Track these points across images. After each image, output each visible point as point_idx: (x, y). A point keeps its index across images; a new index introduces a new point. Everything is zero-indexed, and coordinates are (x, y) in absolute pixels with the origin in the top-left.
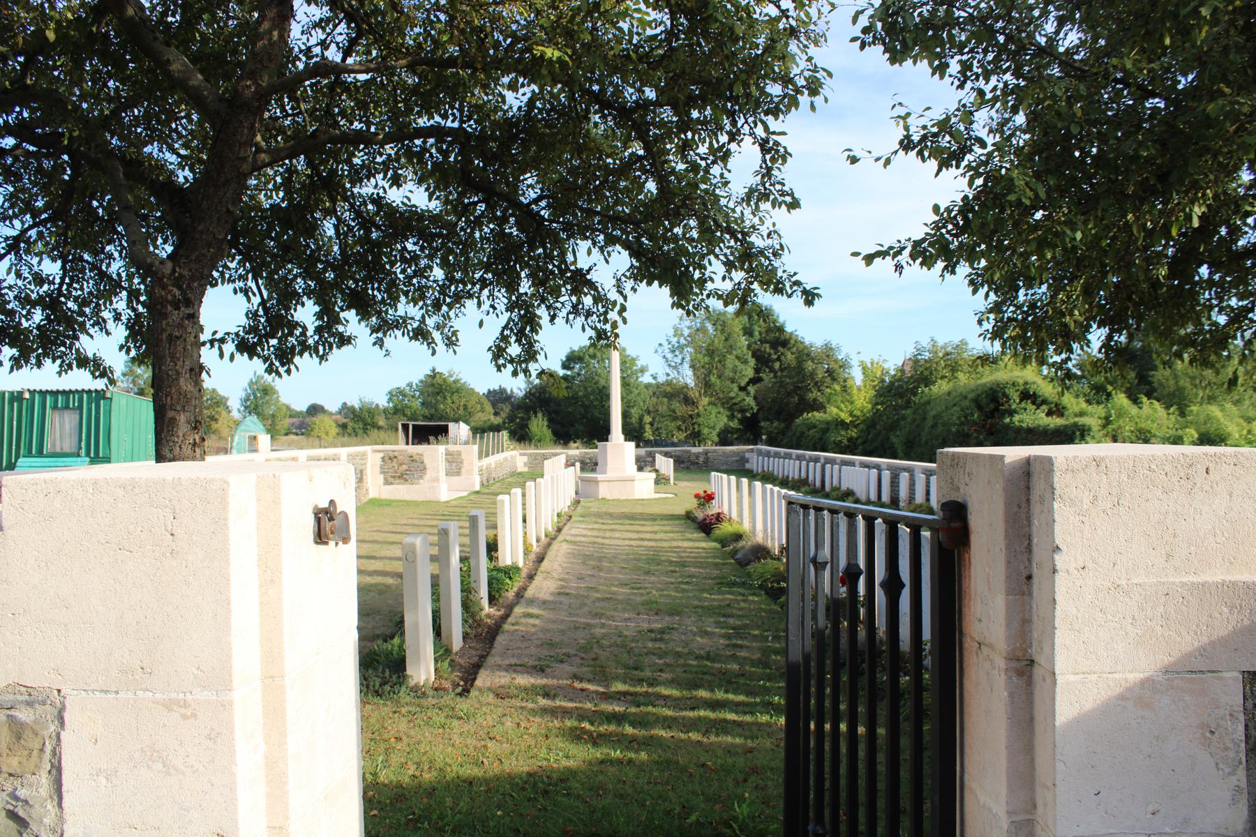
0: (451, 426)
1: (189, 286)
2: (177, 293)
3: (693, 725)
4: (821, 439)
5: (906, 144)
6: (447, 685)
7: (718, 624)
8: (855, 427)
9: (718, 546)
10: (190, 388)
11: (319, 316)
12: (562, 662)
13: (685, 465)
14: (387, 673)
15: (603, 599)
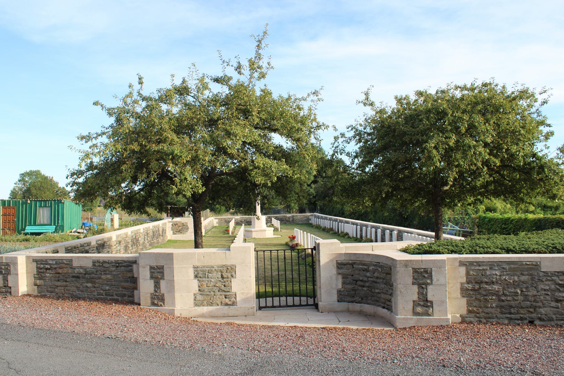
4: (342, 209)
13: (284, 221)
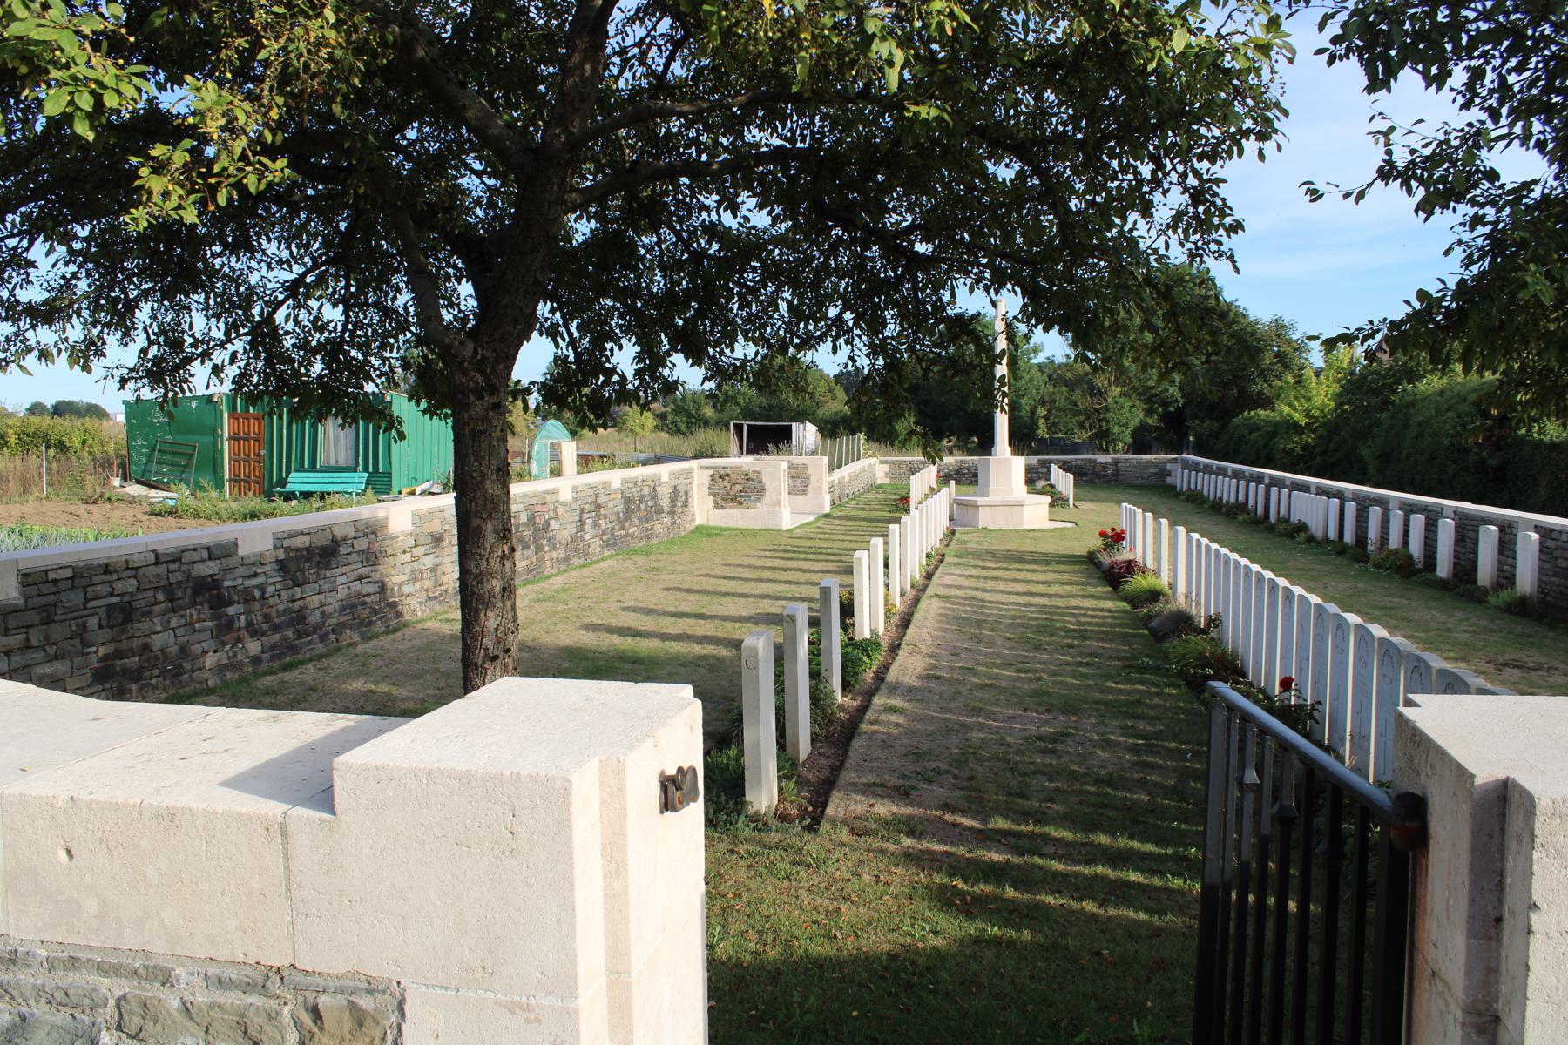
0: (795, 426)
1: (493, 370)
2: (479, 378)
3: (1086, 888)
4: (1266, 445)
5: (1387, 173)
6: (793, 811)
7: (1125, 730)
8: (1313, 431)
9: (1128, 607)
10: (497, 490)
11: (639, 358)
12: (930, 781)
13: (1088, 479)
14: (723, 798)
15: (983, 686)
